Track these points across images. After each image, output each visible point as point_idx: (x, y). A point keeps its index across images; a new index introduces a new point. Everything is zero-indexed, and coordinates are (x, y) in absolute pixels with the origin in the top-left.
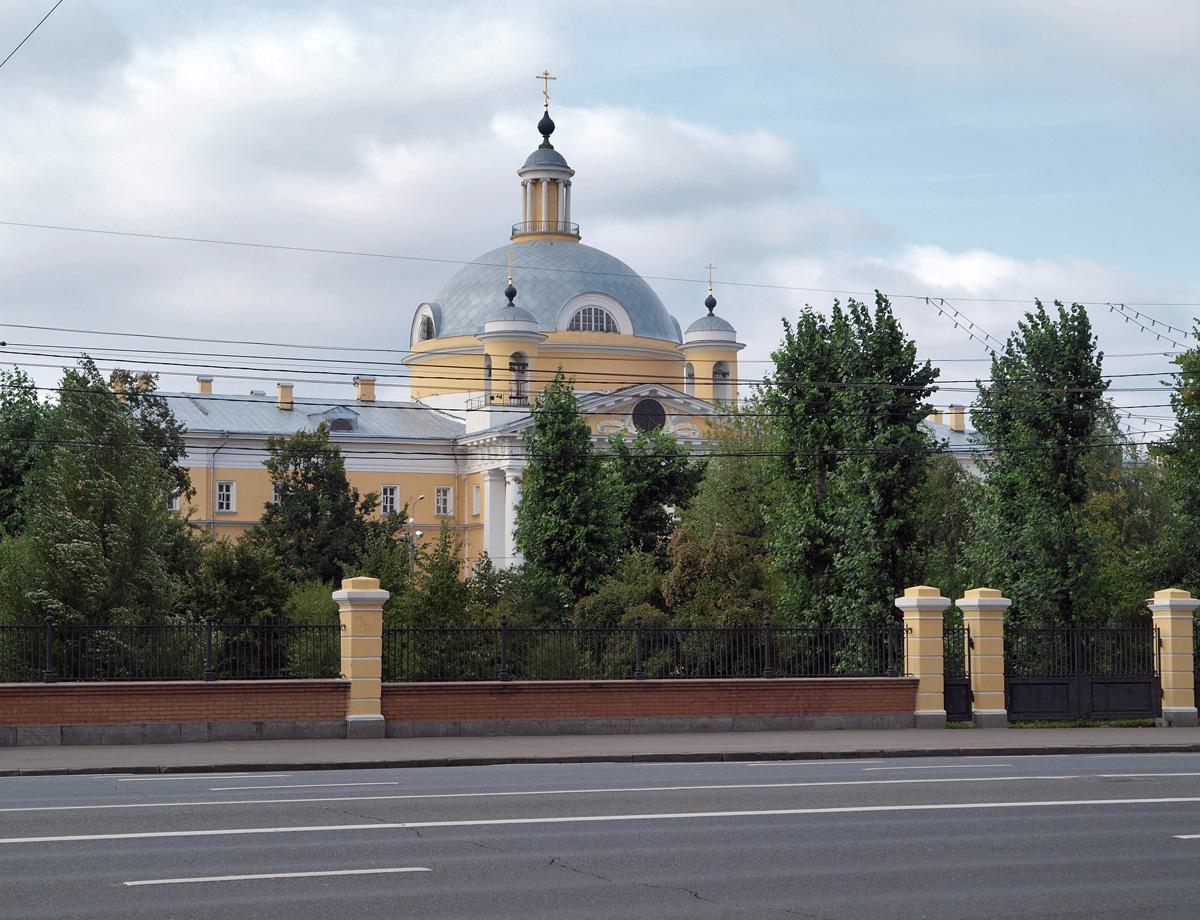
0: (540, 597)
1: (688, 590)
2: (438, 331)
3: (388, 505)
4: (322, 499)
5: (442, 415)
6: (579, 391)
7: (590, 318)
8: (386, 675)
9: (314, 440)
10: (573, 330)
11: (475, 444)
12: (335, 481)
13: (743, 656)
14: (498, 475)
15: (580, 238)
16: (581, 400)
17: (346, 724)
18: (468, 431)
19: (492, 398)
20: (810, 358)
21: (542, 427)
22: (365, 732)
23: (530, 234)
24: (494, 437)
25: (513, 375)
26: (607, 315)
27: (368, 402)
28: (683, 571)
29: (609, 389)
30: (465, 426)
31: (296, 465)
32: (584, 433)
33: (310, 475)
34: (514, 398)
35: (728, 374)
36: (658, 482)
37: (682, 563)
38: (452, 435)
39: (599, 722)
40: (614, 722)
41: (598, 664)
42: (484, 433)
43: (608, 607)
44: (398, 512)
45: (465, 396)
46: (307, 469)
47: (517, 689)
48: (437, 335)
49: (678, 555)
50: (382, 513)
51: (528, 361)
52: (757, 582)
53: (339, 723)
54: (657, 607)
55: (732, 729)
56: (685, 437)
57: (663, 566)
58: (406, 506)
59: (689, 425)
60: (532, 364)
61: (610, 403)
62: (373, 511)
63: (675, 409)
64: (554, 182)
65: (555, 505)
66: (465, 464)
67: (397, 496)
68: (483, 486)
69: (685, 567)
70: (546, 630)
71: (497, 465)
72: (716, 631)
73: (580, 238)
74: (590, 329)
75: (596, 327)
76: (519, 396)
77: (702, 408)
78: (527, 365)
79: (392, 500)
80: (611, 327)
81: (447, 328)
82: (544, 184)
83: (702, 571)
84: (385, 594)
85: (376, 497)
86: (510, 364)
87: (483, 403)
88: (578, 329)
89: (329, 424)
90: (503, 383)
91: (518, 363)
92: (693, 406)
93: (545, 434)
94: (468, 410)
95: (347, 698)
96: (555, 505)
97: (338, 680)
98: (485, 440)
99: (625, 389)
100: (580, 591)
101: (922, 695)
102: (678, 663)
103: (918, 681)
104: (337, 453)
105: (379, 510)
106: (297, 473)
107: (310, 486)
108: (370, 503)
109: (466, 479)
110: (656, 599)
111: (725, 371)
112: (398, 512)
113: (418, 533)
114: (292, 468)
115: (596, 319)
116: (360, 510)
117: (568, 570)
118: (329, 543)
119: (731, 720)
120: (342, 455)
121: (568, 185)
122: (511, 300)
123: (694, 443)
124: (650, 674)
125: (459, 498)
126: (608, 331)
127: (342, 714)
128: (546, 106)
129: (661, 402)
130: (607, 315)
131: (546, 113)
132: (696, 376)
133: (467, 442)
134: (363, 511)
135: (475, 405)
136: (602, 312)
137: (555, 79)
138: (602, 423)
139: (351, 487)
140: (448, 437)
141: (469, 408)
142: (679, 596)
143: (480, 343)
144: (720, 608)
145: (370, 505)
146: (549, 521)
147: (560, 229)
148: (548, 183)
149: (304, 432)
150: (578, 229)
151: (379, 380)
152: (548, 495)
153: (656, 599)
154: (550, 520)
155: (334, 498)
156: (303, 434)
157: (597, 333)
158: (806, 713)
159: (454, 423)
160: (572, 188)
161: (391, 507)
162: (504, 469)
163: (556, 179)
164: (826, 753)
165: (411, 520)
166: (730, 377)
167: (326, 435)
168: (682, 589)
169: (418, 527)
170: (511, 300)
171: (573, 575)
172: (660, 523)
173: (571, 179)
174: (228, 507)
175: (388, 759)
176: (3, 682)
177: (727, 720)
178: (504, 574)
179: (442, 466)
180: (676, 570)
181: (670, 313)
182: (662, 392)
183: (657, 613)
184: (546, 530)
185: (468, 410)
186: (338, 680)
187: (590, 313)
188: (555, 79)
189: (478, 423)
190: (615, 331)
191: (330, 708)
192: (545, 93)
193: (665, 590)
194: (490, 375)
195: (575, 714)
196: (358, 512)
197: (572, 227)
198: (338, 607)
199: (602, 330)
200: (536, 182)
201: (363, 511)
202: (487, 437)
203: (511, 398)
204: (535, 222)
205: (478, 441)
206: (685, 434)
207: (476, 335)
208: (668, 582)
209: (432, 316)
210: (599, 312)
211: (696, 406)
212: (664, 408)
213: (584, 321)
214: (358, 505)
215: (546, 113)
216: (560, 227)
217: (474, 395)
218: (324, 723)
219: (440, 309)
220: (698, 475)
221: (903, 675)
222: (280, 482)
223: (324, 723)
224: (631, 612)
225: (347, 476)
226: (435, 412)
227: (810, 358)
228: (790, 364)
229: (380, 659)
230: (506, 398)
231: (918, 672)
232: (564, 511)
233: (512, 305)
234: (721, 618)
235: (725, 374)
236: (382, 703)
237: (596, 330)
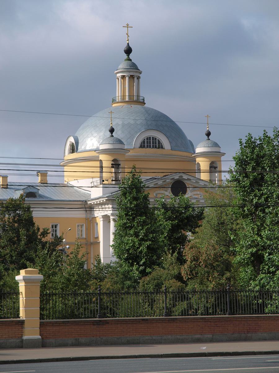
0: (126, 277)
1: (194, 272)
2: (77, 149)
3: (54, 233)
4: (22, 231)
5: (80, 189)
6: (143, 178)
7: (150, 142)
8: (42, 317)
9: (18, 202)
10: (142, 148)
11: (95, 203)
12: (30, 222)
15: (145, 104)
16: (144, 182)
17: (23, 340)
18: (92, 197)
19: (103, 181)
20: (252, 159)
21: (124, 194)
22: (32, 345)
23: (121, 102)
24: (104, 200)
25: (113, 170)
26: (158, 140)
27: (44, 183)
28: (191, 263)
29: (160, 175)
30: (91, 194)
31: (9, 215)
32: (146, 198)
33: (16, 219)
34: (114, 181)
35: (217, 167)
36: (181, 221)
37: (191, 259)
38: (84, 199)
39: (147, 338)
40: (154, 338)
41: (151, 309)
42: (100, 198)
43: (156, 281)
44: (59, 236)
45: (91, 180)
46: (14, 217)
47: (107, 322)
48: (77, 151)
49: (188, 254)
50: (51, 237)
51: (120, 163)
52: (228, 266)
53: (19, 340)
54: (179, 281)
55: (212, 341)
56: (196, 198)
57: (181, 260)
58: (63, 234)
59: (198, 193)
60: (122, 164)
61: (160, 183)
62: (47, 236)
63: (191, 185)
64: (132, 77)
65: (132, 232)
66: (91, 213)
67: (58, 228)
68: (100, 223)
69: (192, 261)
70: (128, 293)
71: (106, 213)
72: (209, 292)
73: (145, 104)
74: (150, 147)
75: (153, 146)
77: (204, 184)
78: (120, 165)
79: (56, 231)
80: (160, 146)
81: (81, 148)
83: (201, 262)
84: (41, 277)
85: (48, 230)
86: (112, 164)
87: (99, 183)
88: (144, 147)
89: (25, 195)
91: (116, 164)
92: (200, 183)
93: (126, 198)
94: (92, 187)
95: (23, 328)
96: (132, 232)
97: (18, 319)
98: (100, 201)
99: (167, 175)
100: (144, 273)
101: (27, 328)
102: (191, 308)
103: (24, 321)
104: (29, 208)
105: (50, 236)
106: (9, 219)
107: (16, 225)
108: (45, 233)
109: (91, 220)
110: (179, 277)
111: (216, 166)
112: (59, 236)
113: (67, 246)
114: (7, 216)
115: (153, 142)
116: (40, 236)
117: (138, 264)
119: (211, 336)
120: (31, 209)
121: (138, 78)
122: (112, 134)
123: (201, 201)
124: (177, 314)
125: (88, 229)
126: (159, 148)
127: (21, 336)
128: (128, 40)
129: (185, 182)
130: (158, 140)
131: (128, 43)
132: (201, 169)
133: (92, 202)
134: (42, 236)
135: (95, 184)
136: (156, 139)
138: (156, 192)
139: (36, 225)
140: (83, 200)
141: (93, 186)
142: (190, 275)
143: (97, 155)
144: (210, 281)
145: (45, 233)
146: (128, 240)
148: (129, 78)
150: (144, 99)
151: (49, 173)
152: (128, 227)
153: (179, 277)
154: (129, 240)
155: (28, 230)
156: (12, 200)
157: (147, 149)
158: (248, 332)
159: (84, 194)
161: (56, 234)
162: (109, 215)
163: (133, 76)
164: (257, 352)
165: (64, 240)
166: (218, 169)
167: (24, 200)
168: (191, 271)
169: (67, 244)
170: (112, 134)
171: (141, 265)
172: (183, 240)
173: (140, 75)
175: (41, 358)
176: (1, 318)
177: (210, 336)
178: (108, 266)
179: (80, 214)
180: (188, 263)
181: (189, 139)
182: (185, 177)
183: (179, 284)
184: (127, 244)
185: (92, 187)
186: (18, 319)
187: (150, 139)
189: (97, 193)
190: (162, 147)
191: (15, 333)
193: (183, 273)
194: (102, 170)
195: (135, 334)
196: (39, 237)
197: (141, 98)
199: (156, 147)
201: (42, 236)
202: (101, 200)
203: (112, 180)
204: (124, 96)
205: (97, 202)
206: (196, 197)
207: (95, 151)
208: (184, 270)
209: (74, 143)
210: (154, 139)
211: (202, 183)
212: (186, 184)
213: (147, 143)
214: (39, 233)
216: (135, 98)
217: (94, 180)
218: (12, 340)
220: (200, 216)
221: (19, 318)
223: (12, 340)
224: (166, 284)
225: (34, 220)
226: (77, 188)
227: (252, 159)
228: (241, 162)
229: (39, 309)
230: (110, 180)
231: (24, 317)
232: (136, 235)
233: (112, 136)
234: (211, 286)
235: (215, 168)
236: (40, 330)
237: (153, 147)
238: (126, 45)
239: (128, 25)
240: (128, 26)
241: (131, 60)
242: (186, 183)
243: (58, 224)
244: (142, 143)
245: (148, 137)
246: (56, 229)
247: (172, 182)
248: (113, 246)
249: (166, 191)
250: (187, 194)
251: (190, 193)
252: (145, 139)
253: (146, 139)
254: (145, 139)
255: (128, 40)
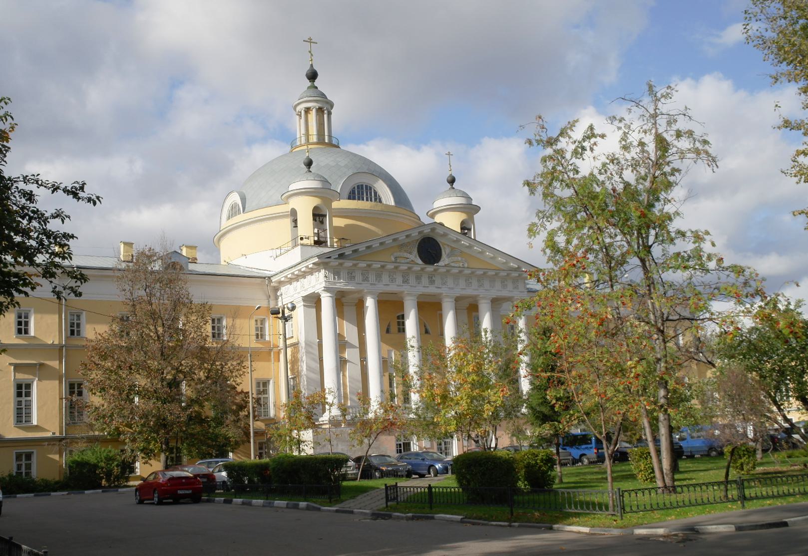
13: (606, 533)
14: (313, 301)
64: (320, 110)
74: (363, 200)
76: (319, 243)
82: (314, 110)
90: (307, 227)
118: (663, 314)
131: (312, 65)
136: (371, 188)
137: (316, 43)
147: (327, 141)
149: (34, 195)
160: (332, 116)
174: (26, 332)
187: (362, 188)
188: (316, 43)
192: (310, 52)
198: (320, 296)
200: (307, 110)
215: (312, 65)
219: (245, 196)
222: (366, 406)
238: (308, 68)
239: (310, 39)
240: (310, 41)
241: (316, 88)
242: (441, 242)
243: (33, 452)
244: (350, 193)
245: (360, 184)
246: (261, 451)
247: (418, 240)
248: (286, 405)
249: (410, 253)
250: (442, 260)
251: (447, 260)
252: (354, 188)
253: (356, 188)
254: (354, 188)
255: (312, 60)
